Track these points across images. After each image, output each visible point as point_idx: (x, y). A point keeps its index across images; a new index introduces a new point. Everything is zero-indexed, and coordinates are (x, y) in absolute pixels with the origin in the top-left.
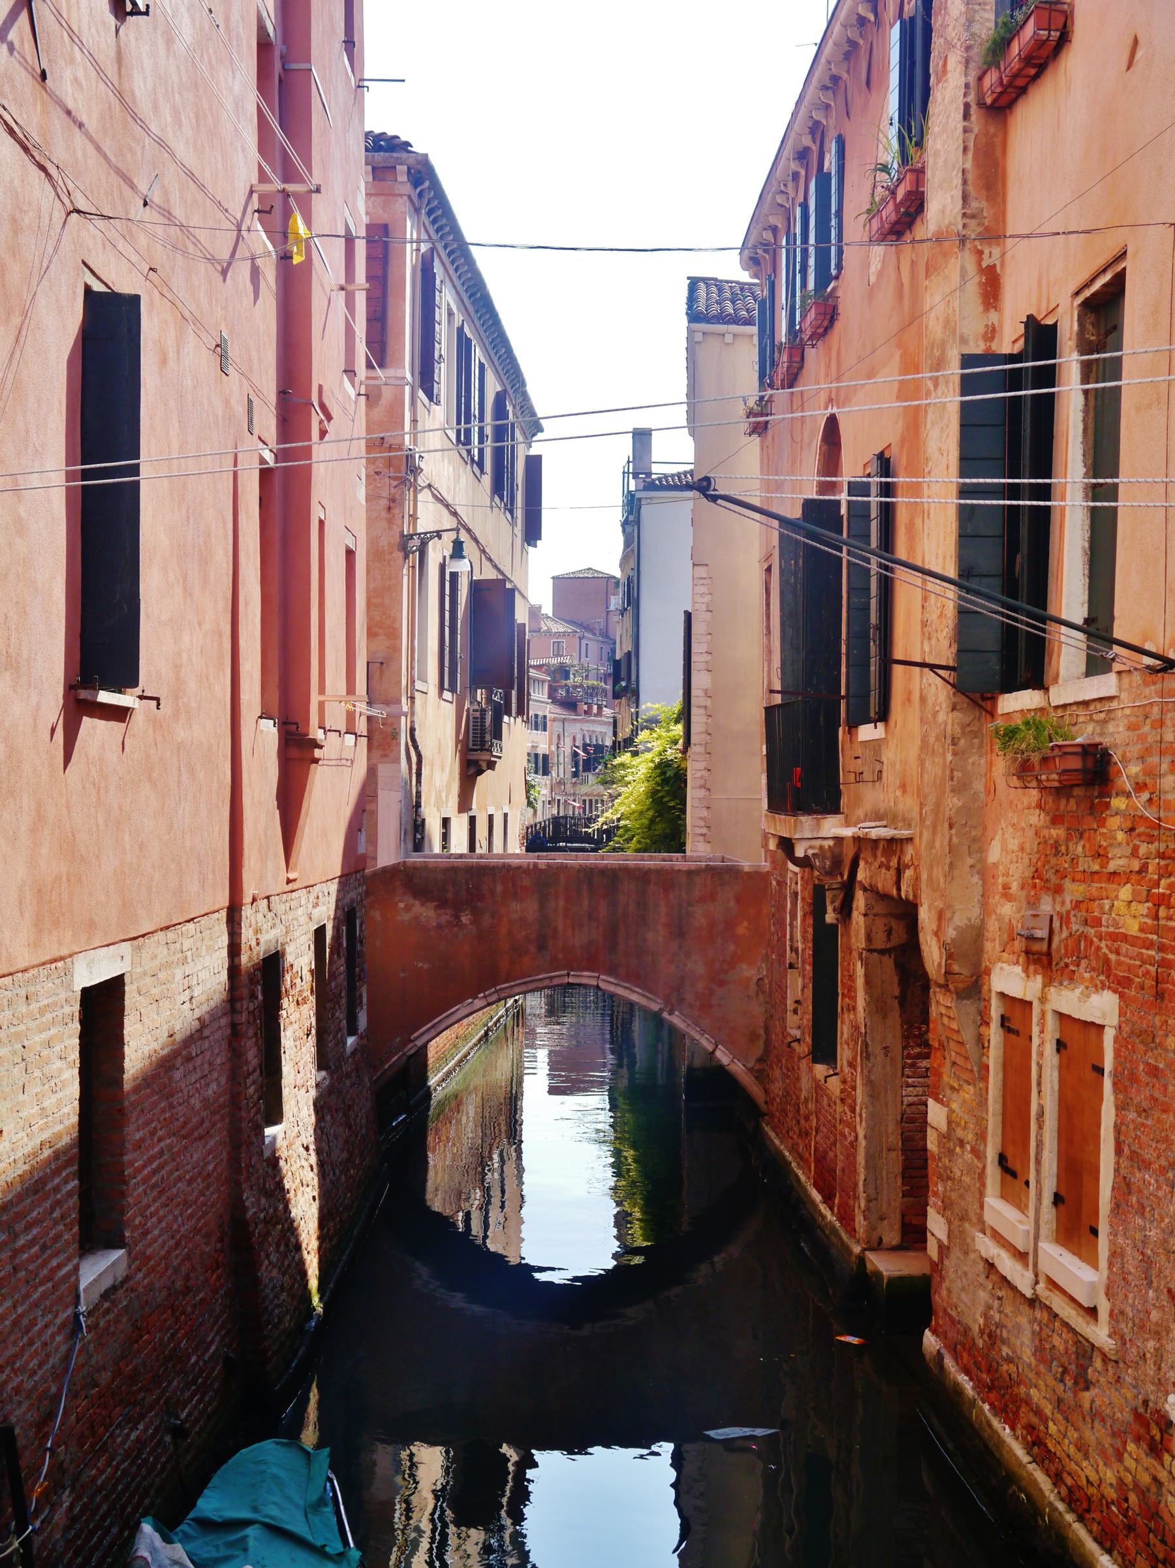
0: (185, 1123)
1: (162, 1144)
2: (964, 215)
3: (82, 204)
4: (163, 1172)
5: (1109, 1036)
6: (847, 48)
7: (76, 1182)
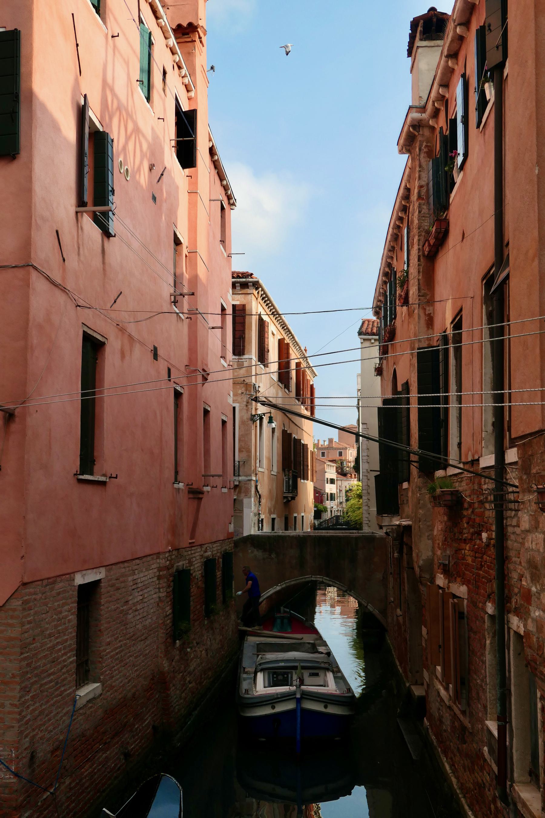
0: (133, 635)
1: (122, 643)
2: (419, 296)
3: (81, 303)
4: (122, 654)
5: (465, 602)
6: (395, 236)
7: (75, 658)
